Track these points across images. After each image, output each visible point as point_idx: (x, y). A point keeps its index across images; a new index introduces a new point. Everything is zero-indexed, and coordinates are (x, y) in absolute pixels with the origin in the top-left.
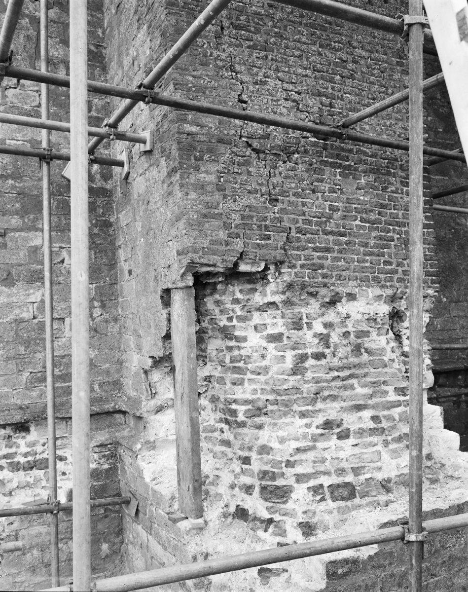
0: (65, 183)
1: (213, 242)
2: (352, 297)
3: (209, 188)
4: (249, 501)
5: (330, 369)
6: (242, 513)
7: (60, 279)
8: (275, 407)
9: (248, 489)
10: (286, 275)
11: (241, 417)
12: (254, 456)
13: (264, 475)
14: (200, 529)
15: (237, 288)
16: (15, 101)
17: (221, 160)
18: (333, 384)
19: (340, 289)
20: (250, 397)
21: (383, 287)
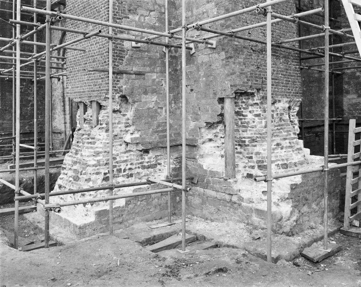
0: (163, 54)
1: (244, 83)
2: (280, 101)
3: (242, 64)
4: (253, 171)
5: (275, 126)
6: (249, 176)
7: (162, 92)
8: (260, 139)
9: (253, 167)
10: (261, 93)
11: (247, 143)
12: (254, 156)
13: (258, 162)
14: (236, 182)
15: (243, 98)
16: (148, 21)
17: (244, 54)
18: (277, 131)
19: (276, 99)
20: (250, 136)
21: (288, 98)
